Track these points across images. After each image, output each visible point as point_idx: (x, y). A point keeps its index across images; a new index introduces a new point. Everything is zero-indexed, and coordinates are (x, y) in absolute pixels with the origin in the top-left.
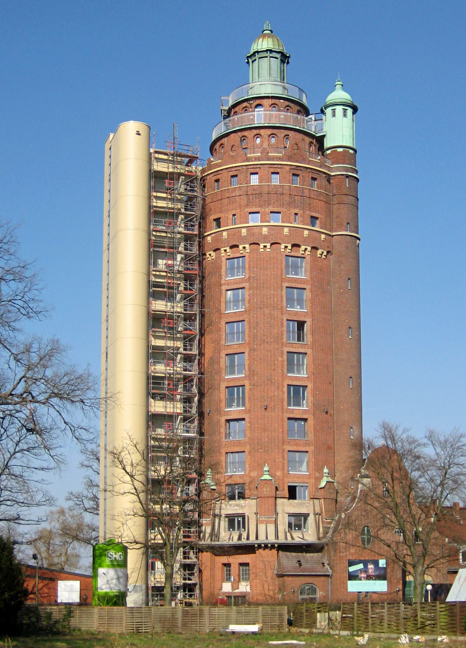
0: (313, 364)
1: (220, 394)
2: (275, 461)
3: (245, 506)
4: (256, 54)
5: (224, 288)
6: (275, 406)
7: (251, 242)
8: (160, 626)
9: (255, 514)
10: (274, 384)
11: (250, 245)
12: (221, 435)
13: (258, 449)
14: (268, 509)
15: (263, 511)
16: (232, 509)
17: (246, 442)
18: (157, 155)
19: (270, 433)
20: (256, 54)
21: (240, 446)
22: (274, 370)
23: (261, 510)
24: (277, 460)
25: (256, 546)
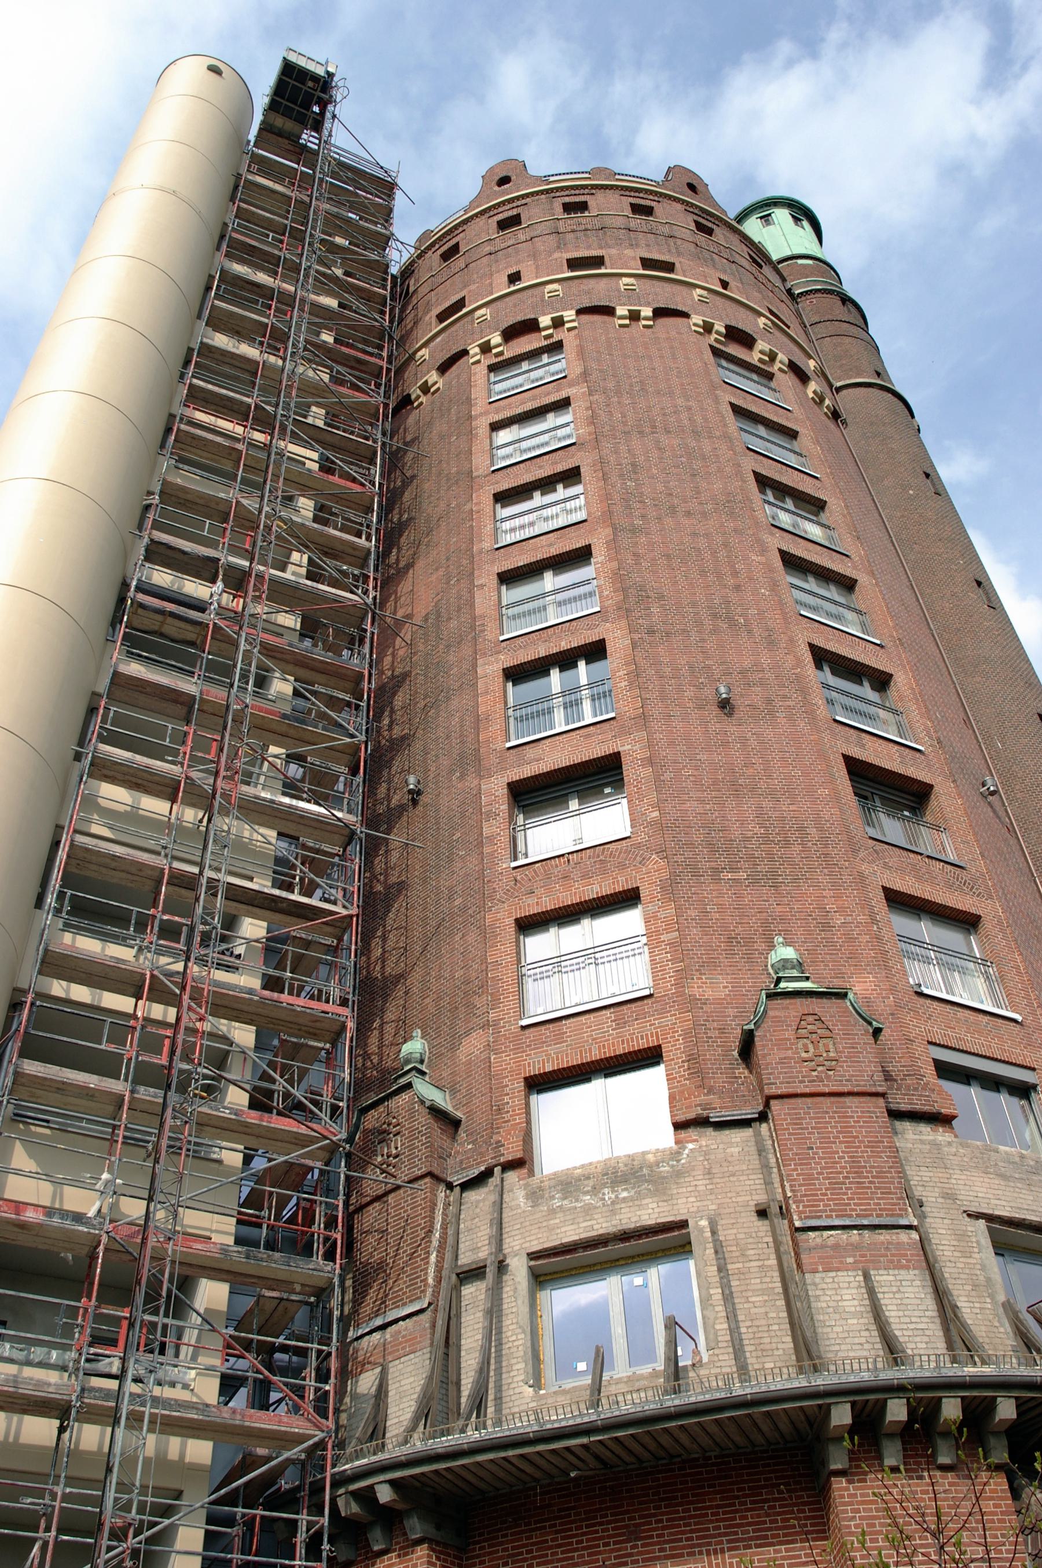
0: (889, 613)
1: (476, 696)
2: (826, 926)
3: (678, 1174)
4: (136, 1095)
5: (482, 425)
6: (769, 701)
7: (587, 303)
8: (516, 1403)
9: (762, 1213)
10: (750, 632)
11: (580, 312)
12: (487, 850)
13: (716, 871)
14: (857, 1170)
15: (822, 1184)
16: (588, 1210)
17: (639, 846)
18: (141, 597)
19: (767, 804)
20: (136, 1095)
21: (604, 872)
22: (737, 588)
23: (809, 1177)
24: (839, 919)
25: (842, 1416)
